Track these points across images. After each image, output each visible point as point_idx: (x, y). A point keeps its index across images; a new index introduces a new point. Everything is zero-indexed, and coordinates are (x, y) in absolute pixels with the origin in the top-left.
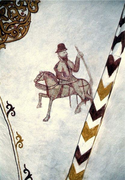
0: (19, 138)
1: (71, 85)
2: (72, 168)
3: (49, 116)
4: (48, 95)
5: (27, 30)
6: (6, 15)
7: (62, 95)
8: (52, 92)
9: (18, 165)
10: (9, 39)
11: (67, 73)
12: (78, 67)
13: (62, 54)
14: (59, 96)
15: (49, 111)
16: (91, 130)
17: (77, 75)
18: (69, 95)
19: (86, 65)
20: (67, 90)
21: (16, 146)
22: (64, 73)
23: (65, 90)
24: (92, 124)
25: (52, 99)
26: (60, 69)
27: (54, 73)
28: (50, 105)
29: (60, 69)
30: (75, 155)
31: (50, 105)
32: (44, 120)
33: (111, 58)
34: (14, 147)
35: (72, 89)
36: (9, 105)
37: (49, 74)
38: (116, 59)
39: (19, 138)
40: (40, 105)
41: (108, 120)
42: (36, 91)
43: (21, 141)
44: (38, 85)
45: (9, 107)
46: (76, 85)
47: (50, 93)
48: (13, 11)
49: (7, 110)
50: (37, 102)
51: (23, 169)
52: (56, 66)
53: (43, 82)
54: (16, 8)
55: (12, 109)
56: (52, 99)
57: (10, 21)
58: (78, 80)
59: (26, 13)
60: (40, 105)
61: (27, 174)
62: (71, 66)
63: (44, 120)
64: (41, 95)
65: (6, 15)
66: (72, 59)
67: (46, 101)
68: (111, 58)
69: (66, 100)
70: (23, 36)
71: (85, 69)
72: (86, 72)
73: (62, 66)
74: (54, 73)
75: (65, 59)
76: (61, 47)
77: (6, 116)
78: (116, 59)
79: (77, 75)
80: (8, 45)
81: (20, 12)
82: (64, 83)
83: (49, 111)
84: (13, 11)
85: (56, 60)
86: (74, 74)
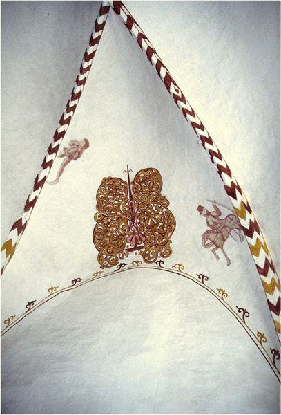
0: (221, 292)
1: (225, 226)
2: (264, 283)
3: (229, 260)
4: (218, 247)
5: (174, 219)
6: (156, 223)
7: (70, 411)
8: (218, 242)
9: (231, 310)
10: (169, 234)
11: (216, 220)
12: (219, 210)
13: (204, 212)
14: (224, 240)
15: (226, 256)
16: (256, 245)
17: (222, 217)
18: (229, 234)
19: (222, 205)
20: (226, 232)
21: (222, 299)
22: (215, 223)
23: (225, 233)
24: (252, 241)
25: (220, 246)
26: (211, 223)
27: (210, 228)
28: (223, 251)
29: (211, 223)
30: (259, 273)
31: (223, 251)
32: (228, 265)
33: (226, 187)
34: (221, 301)
35: (227, 229)
36: (199, 275)
37: (208, 232)
38: (229, 185)
39: (221, 292)
40: (218, 258)
41: (263, 227)
42: (208, 252)
43: (224, 292)
44: (206, 246)
45: (201, 276)
46: (227, 223)
47: (218, 244)
48: (157, 216)
49: (201, 280)
50: (215, 258)
51: (236, 310)
52: (208, 223)
53: (208, 241)
54: (157, 213)
55: (203, 276)
56: (220, 246)
57: (161, 224)
58: (226, 219)
59: (164, 210)
60: (218, 258)
61: (242, 312)
62: (215, 214)
63: (228, 265)
64: (214, 251)
65: (156, 223)
66: (211, 209)
67: (219, 251)
68: (226, 187)
69: (230, 239)
70: (175, 225)
71: (224, 208)
72: (226, 209)
73: (210, 218)
74: (210, 228)
75: (208, 214)
76: (200, 209)
77: (202, 285)
78: (229, 185)
79: (222, 217)
80: (171, 239)
81: (161, 213)
82: (220, 228)
83: (226, 256)
84: (157, 216)
85: (204, 219)
86: (220, 218)
